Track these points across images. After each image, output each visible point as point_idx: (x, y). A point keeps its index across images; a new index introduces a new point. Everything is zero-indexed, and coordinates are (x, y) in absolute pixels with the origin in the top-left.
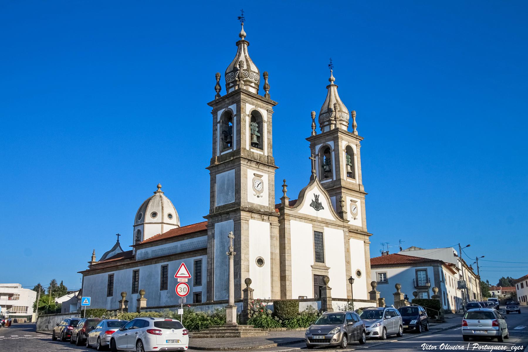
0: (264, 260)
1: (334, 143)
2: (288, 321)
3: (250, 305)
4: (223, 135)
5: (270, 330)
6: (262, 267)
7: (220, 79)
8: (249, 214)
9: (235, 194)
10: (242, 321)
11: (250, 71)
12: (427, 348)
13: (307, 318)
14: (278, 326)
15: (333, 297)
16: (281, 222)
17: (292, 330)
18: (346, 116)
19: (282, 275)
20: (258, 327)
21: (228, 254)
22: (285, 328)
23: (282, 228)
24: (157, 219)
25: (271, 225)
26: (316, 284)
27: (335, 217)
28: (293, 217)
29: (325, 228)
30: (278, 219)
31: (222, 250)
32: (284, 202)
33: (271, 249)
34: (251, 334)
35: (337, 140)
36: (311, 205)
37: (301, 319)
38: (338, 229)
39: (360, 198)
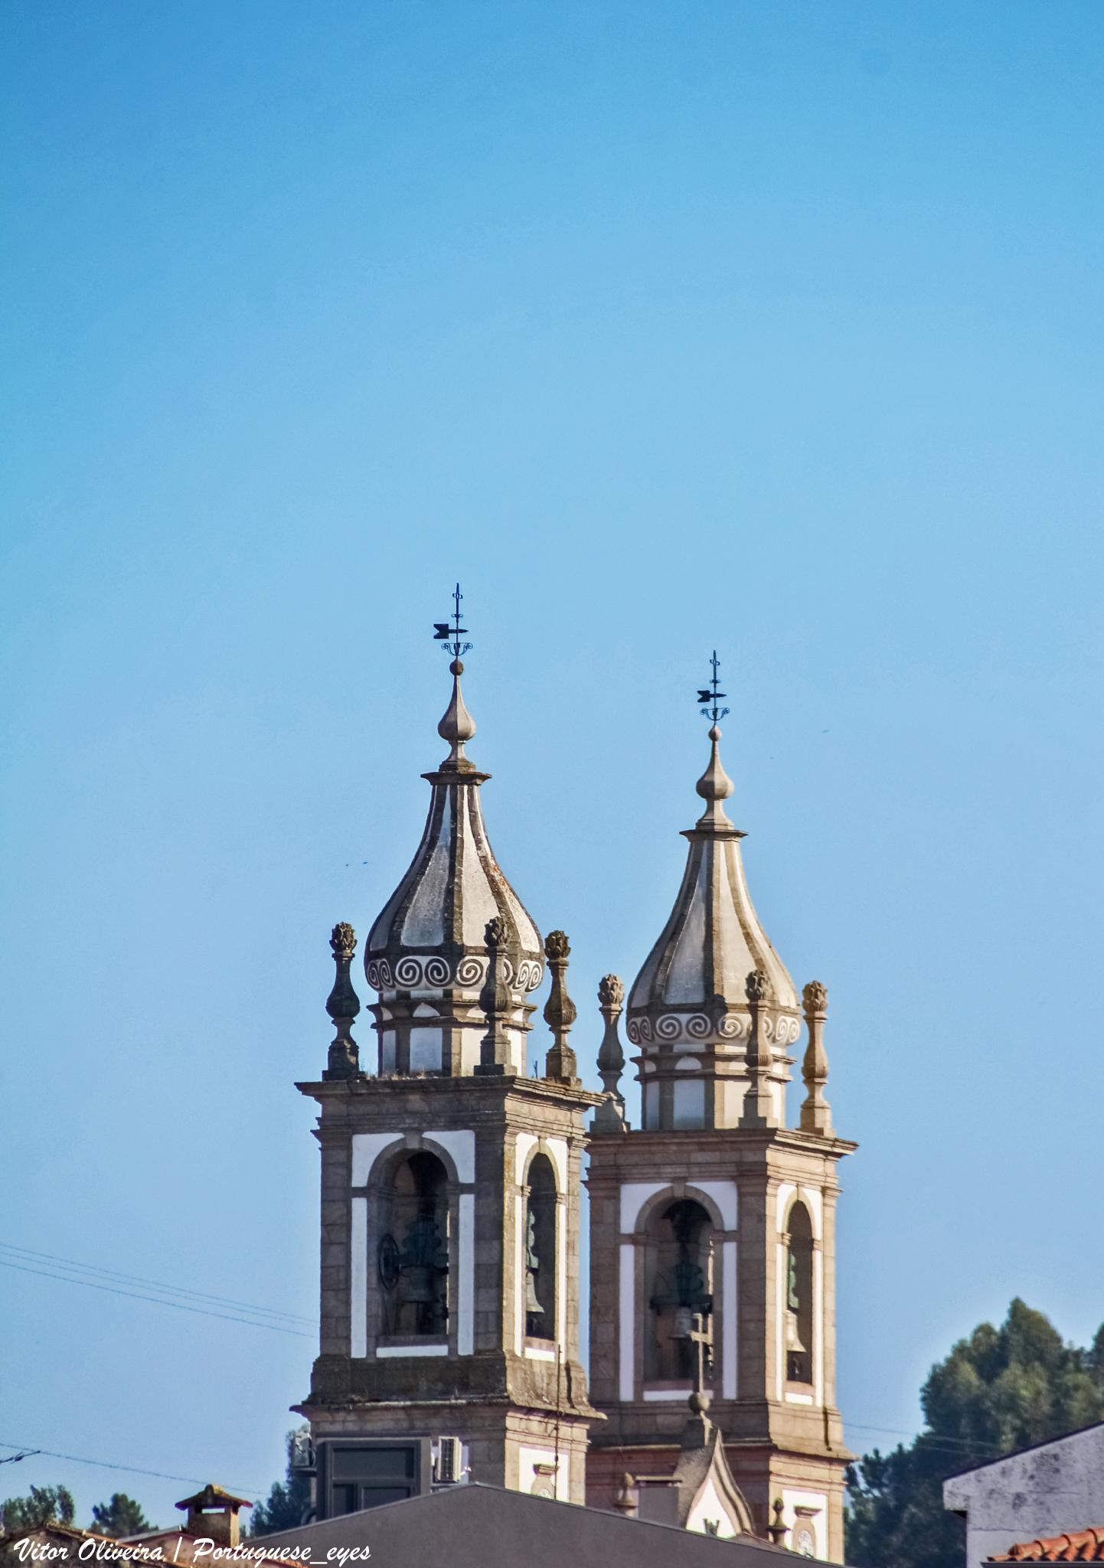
12: (35, 1555)
39: (827, 1487)
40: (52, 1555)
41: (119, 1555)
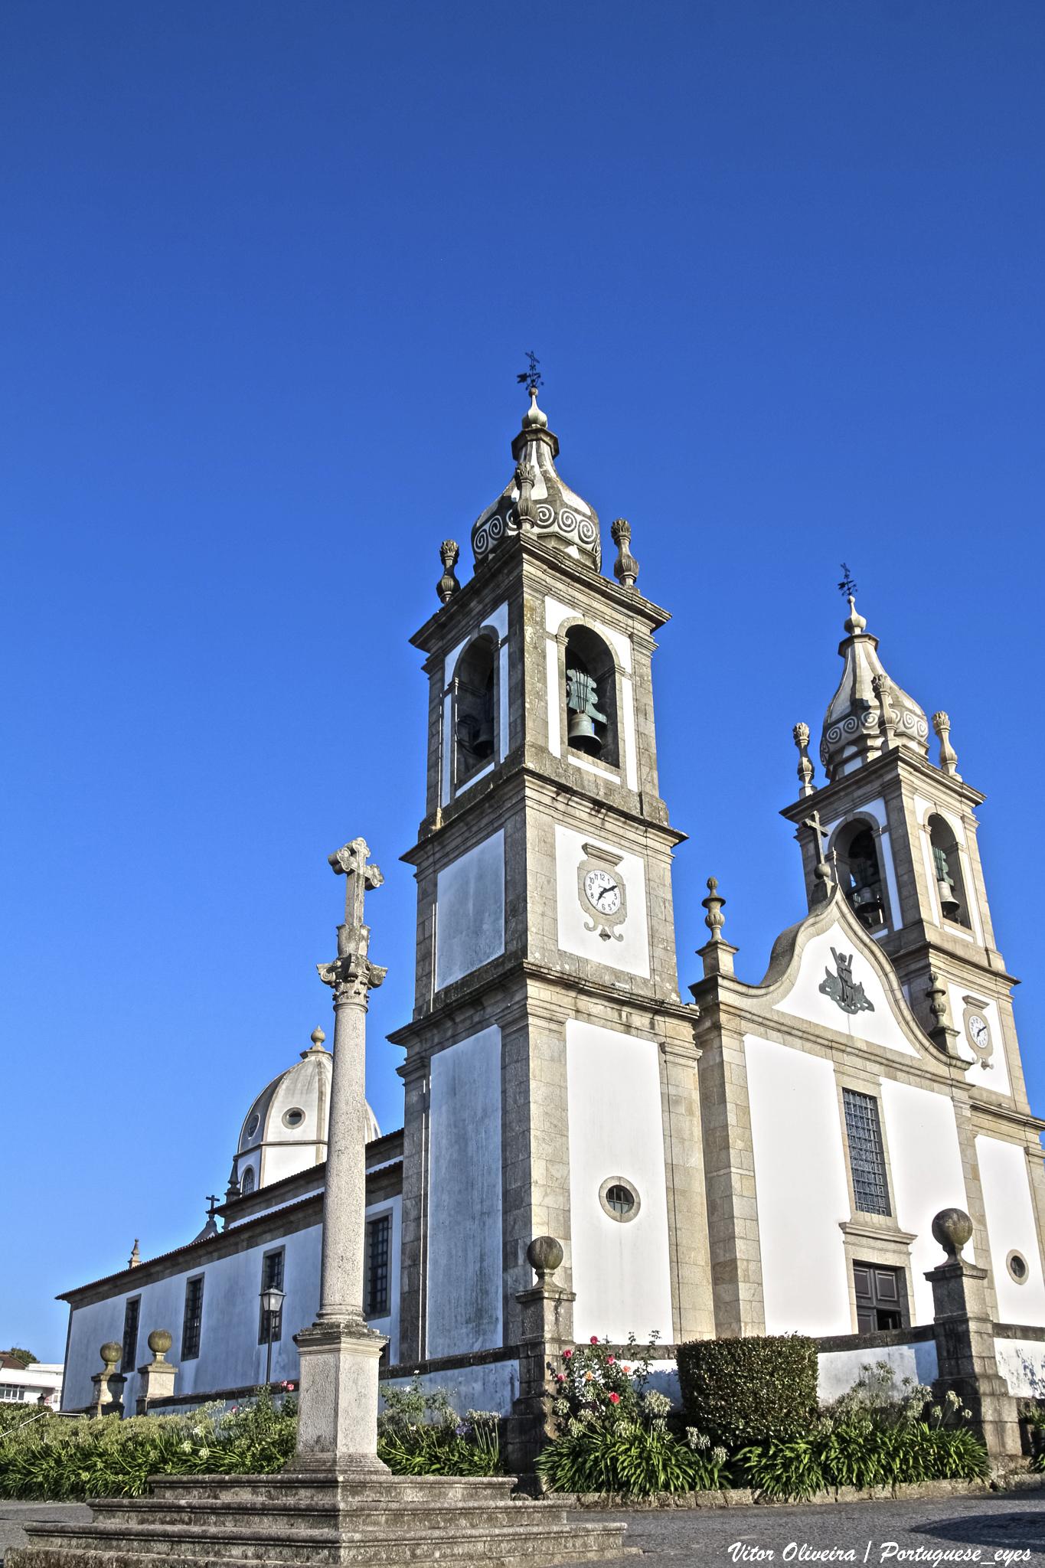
0: (638, 1195)
1: (886, 803)
2: (759, 1450)
3: (553, 1371)
4: (464, 731)
5: (662, 1506)
6: (629, 1220)
7: (455, 562)
8: (565, 998)
9: (506, 922)
10: (513, 1457)
11: (562, 505)
13: (873, 1433)
14: (707, 1483)
15: (1005, 1319)
16: (706, 1041)
17: (786, 1500)
18: (919, 726)
19: (721, 1259)
20: (598, 1490)
21: (333, 977)
22: (749, 1491)
23: (711, 1063)
24: (304, 1131)
25: (664, 1052)
26: (864, 1303)
27: (918, 1045)
28: (753, 1021)
29: (882, 1080)
30: (694, 1032)
31: (455, 1156)
32: (713, 962)
33: (669, 1148)
34: (459, 1550)
35: (894, 791)
36: (822, 989)
37: (833, 1438)
38: (933, 1091)
39: (996, 995)
40: (760, 1556)
41: (818, 1557)
